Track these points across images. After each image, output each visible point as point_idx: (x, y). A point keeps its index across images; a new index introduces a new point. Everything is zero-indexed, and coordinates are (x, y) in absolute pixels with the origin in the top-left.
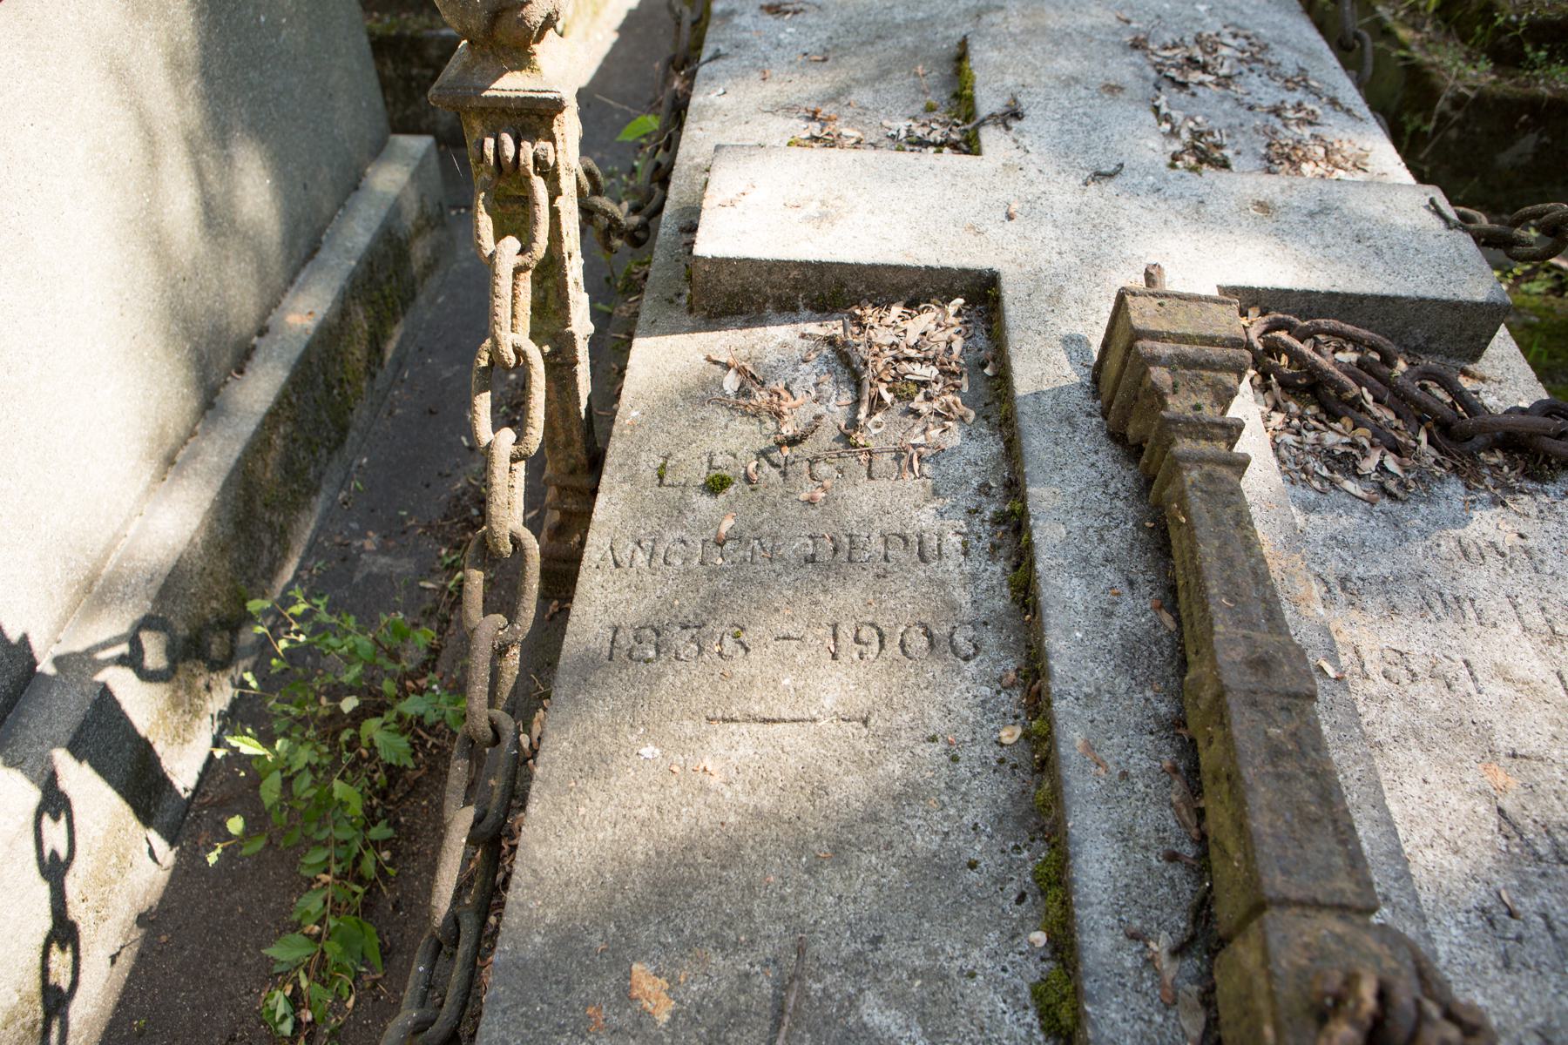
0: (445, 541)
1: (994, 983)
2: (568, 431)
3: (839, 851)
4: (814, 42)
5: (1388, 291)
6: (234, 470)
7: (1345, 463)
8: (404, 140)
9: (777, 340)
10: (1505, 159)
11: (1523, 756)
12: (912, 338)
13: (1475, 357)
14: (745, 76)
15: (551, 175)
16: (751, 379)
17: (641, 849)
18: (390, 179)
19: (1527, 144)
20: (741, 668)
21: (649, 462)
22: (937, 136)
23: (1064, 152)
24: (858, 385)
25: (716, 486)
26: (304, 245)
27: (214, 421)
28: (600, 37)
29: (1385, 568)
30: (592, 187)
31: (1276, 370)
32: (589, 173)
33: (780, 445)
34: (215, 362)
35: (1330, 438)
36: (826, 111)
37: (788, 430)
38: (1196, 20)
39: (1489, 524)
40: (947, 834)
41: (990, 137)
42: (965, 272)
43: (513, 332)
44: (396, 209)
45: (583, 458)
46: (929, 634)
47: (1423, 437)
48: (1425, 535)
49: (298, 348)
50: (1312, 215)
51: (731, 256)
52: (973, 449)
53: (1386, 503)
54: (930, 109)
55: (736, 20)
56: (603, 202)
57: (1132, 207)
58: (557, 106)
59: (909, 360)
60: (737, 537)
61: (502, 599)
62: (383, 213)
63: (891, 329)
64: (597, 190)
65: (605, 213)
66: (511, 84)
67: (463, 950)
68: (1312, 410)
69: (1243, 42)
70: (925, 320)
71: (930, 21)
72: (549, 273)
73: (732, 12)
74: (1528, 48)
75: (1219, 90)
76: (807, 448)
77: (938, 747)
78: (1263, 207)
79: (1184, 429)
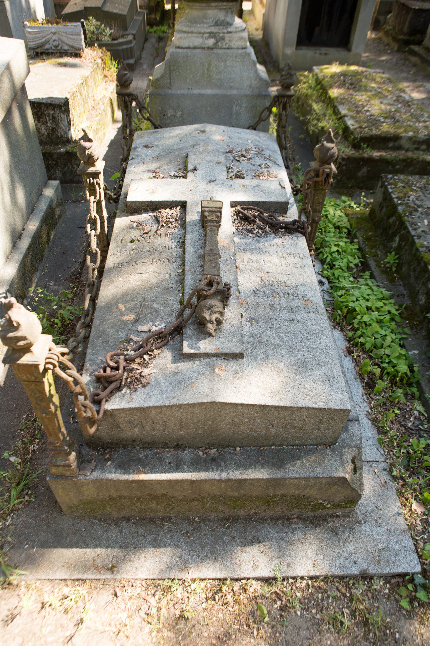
0: (71, 282)
1: (173, 300)
2: (103, 238)
3: (151, 288)
4: (155, 155)
5: (265, 200)
6: (22, 260)
7: (251, 231)
8: (51, 182)
9: (144, 217)
10: (360, 174)
12: (170, 214)
13: (286, 213)
14: (139, 163)
15: (99, 185)
16: (139, 224)
17: (119, 291)
18: (49, 192)
19: (365, 170)
20: (136, 267)
21: (119, 239)
22: (180, 175)
23: (204, 178)
24: (159, 222)
25: (132, 241)
26: (31, 209)
27: (16, 249)
28: (103, 149)
29: (253, 247)
30: (106, 189)
31: (239, 216)
32: (105, 186)
33: (144, 234)
34: (16, 237)
35: (249, 227)
36: (156, 171)
37: (146, 231)
38: (247, 144)
39: (278, 241)
41: (190, 175)
42: (180, 201)
43: (94, 213)
44: (51, 200)
45: (106, 243)
46: (168, 260)
47: (268, 227)
48: (263, 242)
49: (33, 234)
50: (254, 187)
52: (179, 232)
53: (257, 238)
54: (180, 169)
55: (137, 149)
56: (107, 192)
57: (216, 188)
58: (100, 173)
60: (136, 249)
61: (94, 261)
62: (49, 201)
63: (166, 213)
64: (106, 189)
65: (109, 194)
66: (91, 170)
67: (90, 316)
68: (246, 223)
69: (257, 149)
70: (173, 211)
71: (182, 148)
72: (99, 203)
73: (136, 147)
74: (362, 144)
75: (248, 161)
76: (149, 234)
78: (244, 186)
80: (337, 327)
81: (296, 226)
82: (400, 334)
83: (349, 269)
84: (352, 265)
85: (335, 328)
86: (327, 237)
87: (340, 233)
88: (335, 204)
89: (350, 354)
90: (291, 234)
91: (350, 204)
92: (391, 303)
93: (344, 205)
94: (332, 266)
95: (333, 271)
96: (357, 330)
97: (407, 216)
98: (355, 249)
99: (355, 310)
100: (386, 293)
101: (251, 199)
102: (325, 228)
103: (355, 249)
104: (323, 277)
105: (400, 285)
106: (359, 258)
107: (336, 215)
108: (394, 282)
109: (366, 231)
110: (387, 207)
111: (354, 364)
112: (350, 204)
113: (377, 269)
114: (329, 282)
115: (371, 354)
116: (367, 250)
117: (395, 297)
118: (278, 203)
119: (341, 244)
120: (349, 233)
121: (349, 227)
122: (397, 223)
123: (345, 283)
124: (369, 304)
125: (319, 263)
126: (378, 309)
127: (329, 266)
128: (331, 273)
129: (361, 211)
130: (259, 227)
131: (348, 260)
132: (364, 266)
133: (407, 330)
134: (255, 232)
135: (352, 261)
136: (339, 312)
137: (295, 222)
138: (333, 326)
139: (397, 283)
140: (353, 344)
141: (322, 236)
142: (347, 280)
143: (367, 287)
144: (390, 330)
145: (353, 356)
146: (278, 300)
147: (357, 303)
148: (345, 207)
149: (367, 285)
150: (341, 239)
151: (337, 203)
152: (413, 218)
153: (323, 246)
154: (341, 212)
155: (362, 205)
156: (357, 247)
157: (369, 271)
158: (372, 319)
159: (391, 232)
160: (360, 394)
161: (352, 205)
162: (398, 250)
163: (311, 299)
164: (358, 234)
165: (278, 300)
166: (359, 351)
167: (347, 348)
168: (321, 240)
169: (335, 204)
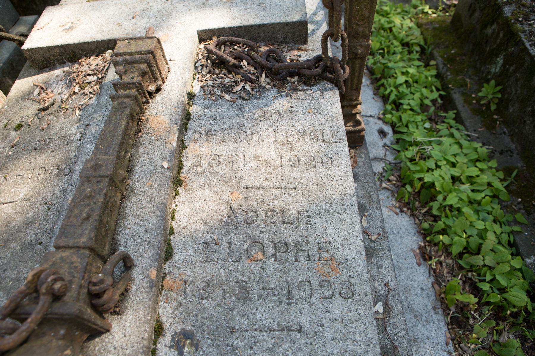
5: (258, 21)
7: (228, 89)
11: (250, 188)
13: (305, 42)
35: (226, 80)
39: (282, 104)
40: (37, 234)
47: (264, 75)
51: (33, 47)
53: (240, 102)
59: (89, 75)
68: (224, 71)
77: (46, 206)
79: (120, 87)
80: (405, 209)
81: (319, 70)
82: (509, 223)
83: (424, 108)
84: (427, 102)
85: (402, 211)
86: (390, 61)
87: (410, 52)
88: (403, 11)
89: (425, 260)
90: (311, 85)
91: (423, 9)
92: (491, 168)
93: (415, 11)
94: (397, 106)
95: (399, 113)
96: (436, 219)
97: (521, 23)
98: (432, 76)
99: (433, 185)
100: (484, 151)
101: (235, 23)
102: (388, 47)
103: (432, 76)
104: (386, 123)
105: (504, 133)
106: (438, 90)
107: (404, 26)
108: (494, 128)
109: (447, 47)
110: (482, 10)
111: (432, 279)
112: (423, 9)
113: (466, 107)
114: (395, 132)
115: (460, 262)
116: (449, 77)
117: (497, 154)
118: (287, 24)
119: (412, 71)
120: (423, 50)
121: (422, 43)
122: (501, 35)
123: (419, 136)
124: (456, 172)
125: (380, 100)
126: (470, 179)
127: (394, 106)
128: (397, 117)
129: (440, 18)
130: (247, 79)
131: (422, 94)
132: (447, 103)
133: (519, 217)
134: (238, 88)
135: (428, 96)
136: (408, 188)
137: (318, 59)
138: (399, 208)
139: (499, 130)
140: (429, 242)
141: (383, 61)
142: (420, 127)
143: (451, 140)
144: (492, 218)
145: (430, 265)
146: (259, 265)
147: (437, 173)
148: (417, 14)
149: (452, 135)
150: (411, 63)
151: (405, 9)
152: (530, 25)
153: (386, 74)
154: (412, 21)
155: (440, 8)
156: (434, 72)
157: (453, 110)
158: (461, 199)
159: (488, 49)
160: (442, 340)
161: (425, 11)
162: (501, 79)
163: (339, 254)
164: (435, 53)
165: (259, 265)
166: (440, 253)
167: (420, 248)
168: (382, 66)
169: (403, 11)
